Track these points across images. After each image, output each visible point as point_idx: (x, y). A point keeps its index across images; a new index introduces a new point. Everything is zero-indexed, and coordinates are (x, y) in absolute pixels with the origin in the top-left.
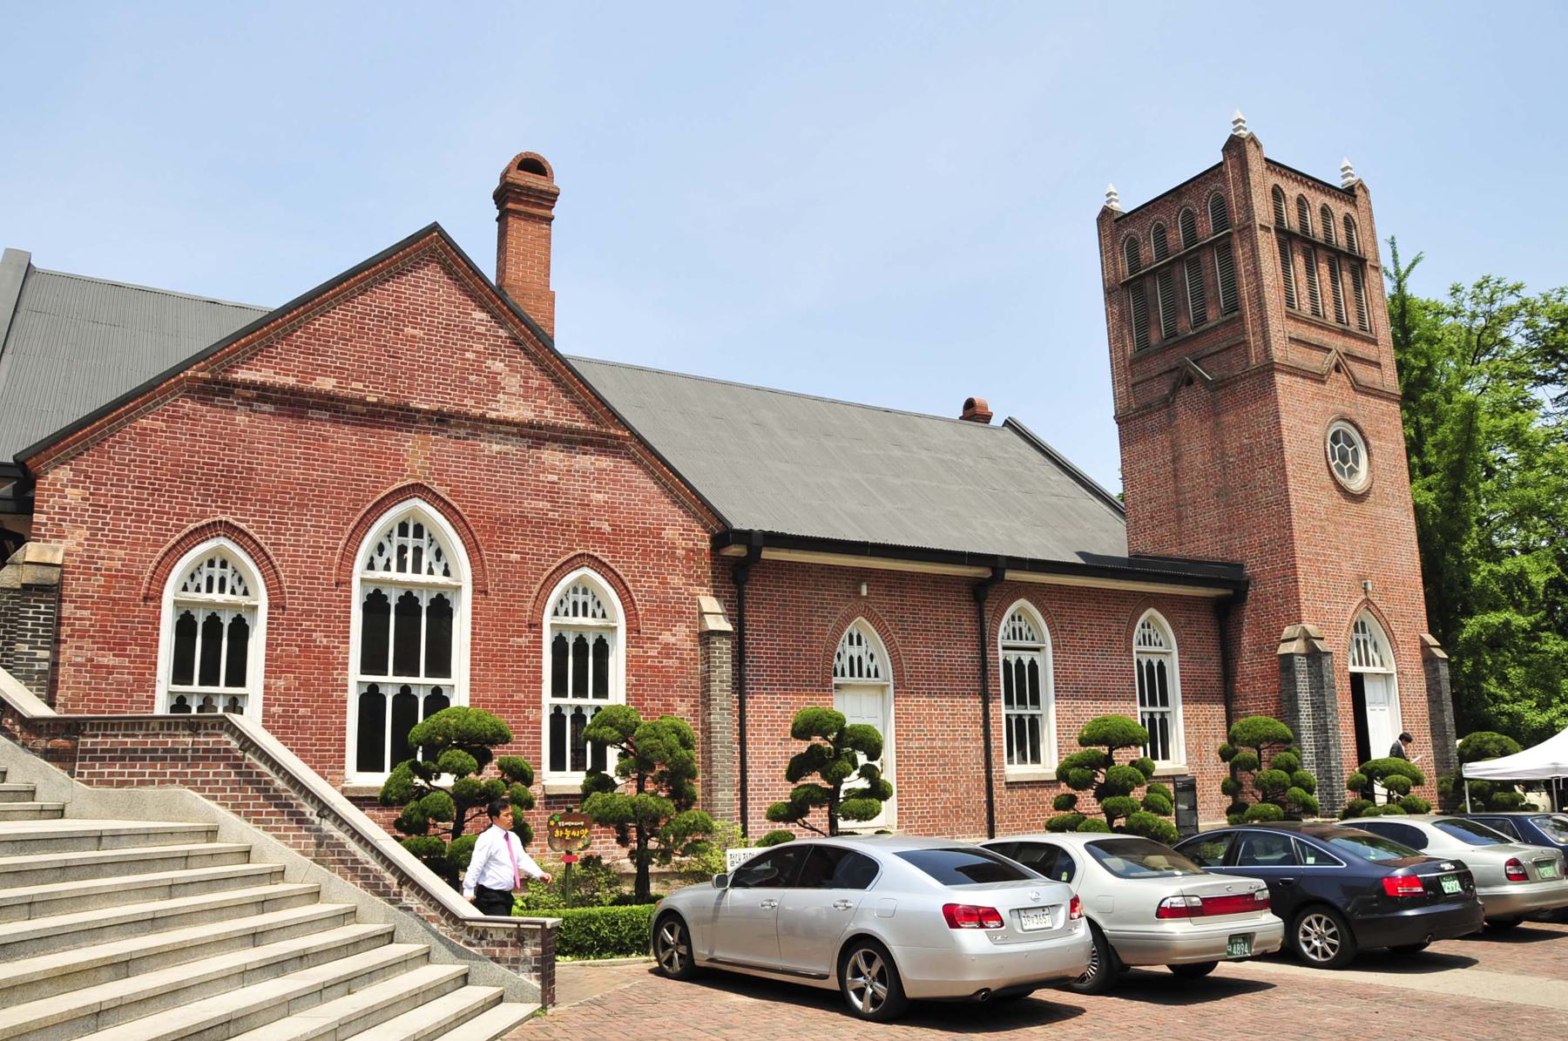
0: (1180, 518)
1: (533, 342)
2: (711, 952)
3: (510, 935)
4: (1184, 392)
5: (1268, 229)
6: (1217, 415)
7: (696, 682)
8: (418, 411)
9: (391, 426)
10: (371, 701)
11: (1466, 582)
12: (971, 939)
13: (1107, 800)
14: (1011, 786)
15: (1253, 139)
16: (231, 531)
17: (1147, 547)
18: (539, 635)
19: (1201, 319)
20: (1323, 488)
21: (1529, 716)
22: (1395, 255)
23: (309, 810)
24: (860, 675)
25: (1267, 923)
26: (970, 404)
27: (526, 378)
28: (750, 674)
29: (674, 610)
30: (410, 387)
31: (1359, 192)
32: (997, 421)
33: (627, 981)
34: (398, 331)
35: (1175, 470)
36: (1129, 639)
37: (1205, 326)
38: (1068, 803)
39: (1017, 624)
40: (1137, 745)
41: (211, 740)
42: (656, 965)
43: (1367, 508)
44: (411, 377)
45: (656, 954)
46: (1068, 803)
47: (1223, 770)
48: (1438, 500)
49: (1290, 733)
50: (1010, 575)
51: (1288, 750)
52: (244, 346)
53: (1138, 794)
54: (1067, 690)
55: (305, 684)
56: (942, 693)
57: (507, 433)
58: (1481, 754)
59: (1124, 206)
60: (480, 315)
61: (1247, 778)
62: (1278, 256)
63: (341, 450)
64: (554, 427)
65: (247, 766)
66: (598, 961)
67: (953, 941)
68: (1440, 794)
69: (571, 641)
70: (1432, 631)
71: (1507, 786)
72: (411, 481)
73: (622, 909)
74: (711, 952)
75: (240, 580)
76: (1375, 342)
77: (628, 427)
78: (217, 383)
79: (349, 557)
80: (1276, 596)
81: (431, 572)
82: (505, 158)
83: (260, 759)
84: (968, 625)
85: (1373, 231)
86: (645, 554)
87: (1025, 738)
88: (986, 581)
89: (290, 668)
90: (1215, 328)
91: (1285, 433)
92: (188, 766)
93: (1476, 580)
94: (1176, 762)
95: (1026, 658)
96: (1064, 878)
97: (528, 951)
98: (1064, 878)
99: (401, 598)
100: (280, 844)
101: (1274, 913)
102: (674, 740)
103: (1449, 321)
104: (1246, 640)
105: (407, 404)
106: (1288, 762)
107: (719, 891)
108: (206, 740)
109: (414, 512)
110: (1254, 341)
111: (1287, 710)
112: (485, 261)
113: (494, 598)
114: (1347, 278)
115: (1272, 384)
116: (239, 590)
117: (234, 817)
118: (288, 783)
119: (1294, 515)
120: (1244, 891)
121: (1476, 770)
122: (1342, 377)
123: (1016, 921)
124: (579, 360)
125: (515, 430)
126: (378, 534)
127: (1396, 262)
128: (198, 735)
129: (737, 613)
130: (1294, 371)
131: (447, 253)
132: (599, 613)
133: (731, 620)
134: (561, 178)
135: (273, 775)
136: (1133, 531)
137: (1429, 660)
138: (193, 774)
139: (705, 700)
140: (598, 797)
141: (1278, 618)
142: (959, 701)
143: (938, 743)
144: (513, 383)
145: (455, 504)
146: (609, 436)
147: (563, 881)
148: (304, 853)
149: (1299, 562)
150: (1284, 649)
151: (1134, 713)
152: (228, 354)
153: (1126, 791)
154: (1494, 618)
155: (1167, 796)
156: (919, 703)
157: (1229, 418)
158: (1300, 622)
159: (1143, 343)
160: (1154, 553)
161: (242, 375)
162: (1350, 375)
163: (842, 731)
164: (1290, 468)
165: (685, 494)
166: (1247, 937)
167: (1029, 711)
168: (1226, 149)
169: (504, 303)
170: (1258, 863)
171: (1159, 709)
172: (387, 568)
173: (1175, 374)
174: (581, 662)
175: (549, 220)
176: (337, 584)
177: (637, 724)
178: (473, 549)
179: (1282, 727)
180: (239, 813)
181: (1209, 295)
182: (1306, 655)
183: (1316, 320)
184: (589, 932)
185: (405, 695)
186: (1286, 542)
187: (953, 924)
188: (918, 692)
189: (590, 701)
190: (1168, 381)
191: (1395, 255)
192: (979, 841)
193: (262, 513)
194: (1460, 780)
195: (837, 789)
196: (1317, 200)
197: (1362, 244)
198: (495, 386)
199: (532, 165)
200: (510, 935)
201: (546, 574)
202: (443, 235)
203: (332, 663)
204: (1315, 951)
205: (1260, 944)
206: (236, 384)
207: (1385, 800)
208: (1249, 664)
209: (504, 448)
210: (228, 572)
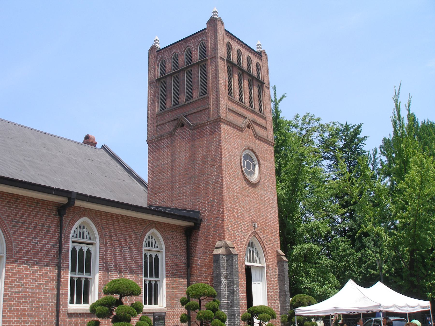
0: (172, 189)
4: (180, 130)
11: (295, 231)
14: (71, 315)
15: (221, 20)
17: (157, 202)
20: (238, 179)
21: (317, 288)
22: (275, 93)
26: (87, 137)
31: (263, 55)
32: (99, 146)
35: (172, 166)
39: (82, 230)
43: (257, 190)
48: (286, 194)
49: (216, 293)
50: (78, 203)
51: (214, 300)
58: (301, 304)
61: (194, 315)
68: (282, 322)
70: (282, 249)
71: (309, 318)
76: (265, 119)
84: (53, 227)
85: (268, 72)
87: (80, 291)
88: (65, 205)
90: (196, 101)
91: (223, 151)
93: (299, 230)
95: (85, 248)
103: (294, 129)
106: (214, 307)
110: (213, 108)
111: (215, 281)
114: (255, 89)
115: (219, 128)
119: (224, 189)
121: (302, 311)
122: (250, 131)
127: (275, 96)
130: (229, 124)
136: (150, 195)
137: (280, 261)
141: (214, 237)
142: (44, 268)
149: (225, 211)
150: (216, 252)
154: (306, 246)
156: (21, 268)
157: (198, 143)
158: (224, 239)
159: (163, 107)
160: (159, 205)
162: (254, 130)
164: (224, 167)
167: (84, 276)
168: (209, 23)
171: (154, 279)
173: (176, 122)
179: (212, 290)
181: (194, 86)
182: (226, 256)
188: (20, 261)
190: (173, 124)
191: (275, 93)
194: (293, 315)
196: (246, 54)
197: (263, 76)
208: (199, 259)
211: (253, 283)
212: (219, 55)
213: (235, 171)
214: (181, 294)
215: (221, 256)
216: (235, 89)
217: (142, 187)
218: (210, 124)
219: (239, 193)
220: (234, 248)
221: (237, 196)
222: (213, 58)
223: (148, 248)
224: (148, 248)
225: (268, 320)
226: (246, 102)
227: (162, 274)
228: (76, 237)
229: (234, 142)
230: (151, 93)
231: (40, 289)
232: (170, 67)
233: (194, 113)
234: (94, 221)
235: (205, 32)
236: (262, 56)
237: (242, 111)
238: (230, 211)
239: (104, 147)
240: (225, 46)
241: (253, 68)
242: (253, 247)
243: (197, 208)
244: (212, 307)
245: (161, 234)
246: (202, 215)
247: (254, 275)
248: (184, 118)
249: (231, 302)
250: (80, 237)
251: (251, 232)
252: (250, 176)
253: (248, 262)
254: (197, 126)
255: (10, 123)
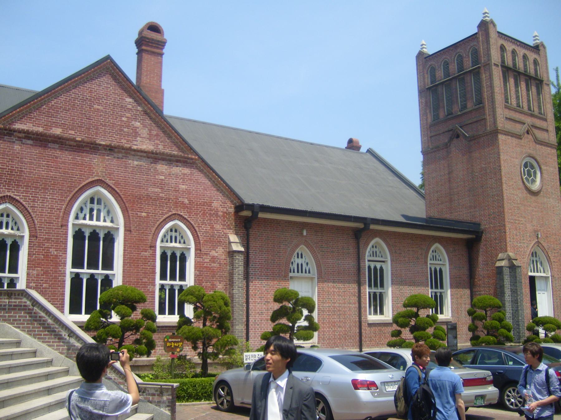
0: (451, 201)
1: (152, 111)
2: (243, 399)
3: (156, 391)
4: (455, 141)
5: (497, 66)
6: (470, 152)
7: (226, 274)
8: (100, 145)
9: (87, 152)
10: (76, 280)
12: (364, 395)
13: (416, 333)
14: (371, 325)
15: (492, 22)
16: (12, 200)
17: (435, 214)
18: (155, 251)
19: (464, 107)
20: (519, 189)
23: (64, 334)
24: (302, 272)
25: (491, 390)
26: (350, 141)
27: (150, 130)
28: (251, 271)
29: (216, 241)
30: (97, 133)
31: (541, 48)
32: (363, 150)
33: (203, 412)
34: (91, 107)
35: (449, 178)
36: (426, 257)
37: (466, 111)
38: (397, 334)
39: (375, 249)
40: (430, 308)
41: (18, 301)
42: (216, 405)
43: (540, 199)
44: (97, 129)
45: (216, 400)
46: (397, 334)
47: (468, 320)
49: (500, 304)
50: (372, 227)
51: (499, 312)
52: (19, 112)
53: (430, 331)
54: (397, 281)
55: (46, 273)
56: (340, 282)
57: (141, 156)
59: (430, 50)
60: (129, 100)
62: (502, 79)
63: (64, 163)
64: (163, 154)
65: (35, 313)
66: (187, 403)
67: (357, 397)
69: (169, 254)
72: (96, 178)
73: (198, 380)
74: (243, 399)
75: (16, 223)
76: (546, 120)
77: (197, 154)
78: (6, 130)
79: (67, 213)
80: (495, 239)
81: (105, 221)
82: (142, 24)
83: (41, 310)
86: (204, 214)
87: (377, 302)
88: (360, 230)
89: (39, 265)
90: (471, 112)
91: (502, 162)
92: (7, 313)
94: (446, 315)
95: (378, 265)
96: (402, 368)
97: (165, 398)
98: (402, 368)
99: (91, 233)
100: (50, 349)
101: (495, 386)
102: (222, 303)
104: (481, 259)
105: (95, 142)
106: (499, 318)
107: (246, 372)
108: (15, 301)
109: (98, 192)
110: (489, 119)
111: (499, 292)
112: (131, 73)
113: (134, 234)
114: (534, 89)
115: (497, 139)
116: (15, 228)
117: (28, 336)
118: (54, 321)
119: (505, 201)
120: (482, 376)
122: (530, 137)
123: (383, 387)
124: (171, 117)
125: (145, 155)
126: (81, 202)
128: (11, 298)
129: (246, 243)
130: (507, 133)
131: (114, 69)
132: (182, 241)
133: (243, 246)
134: (168, 35)
135: (47, 318)
136: (429, 205)
138: (9, 316)
139: (231, 283)
140: (185, 328)
141: (496, 250)
143: (337, 305)
144: (144, 132)
145: (116, 189)
146: (188, 158)
147: (171, 366)
148: (61, 353)
150: (498, 264)
151: (429, 292)
152: (11, 116)
153: (424, 329)
155: (443, 331)
158: (506, 251)
160: (438, 217)
161: (18, 126)
162: (534, 135)
163: (297, 300)
164: (504, 179)
165: (223, 186)
166: (482, 397)
167: (379, 290)
169: (141, 94)
170: (486, 364)
171: (439, 290)
172: (84, 218)
173: (451, 133)
174: (174, 263)
175: (161, 55)
176: (62, 226)
177: (204, 295)
178: (125, 211)
179: (497, 301)
180: (30, 335)
182: (509, 267)
183: (518, 109)
184: (183, 390)
185: (92, 279)
186: (501, 214)
187: (356, 388)
188: (328, 281)
189: (178, 282)
192: (355, 351)
193: (27, 192)
195: (293, 326)
196: (521, 52)
197: (541, 73)
198: (136, 134)
199: (154, 28)
200: (156, 391)
201: (158, 223)
202: (112, 61)
203: (59, 263)
204: (512, 404)
205: (487, 400)
206: (15, 131)
207: (544, 335)
208: (482, 270)
209: (140, 163)
210: (10, 220)
211: (537, 292)
212: (493, 62)
213: (515, 182)
214: (465, 304)
215: (504, 268)
216: (512, 95)
217: (412, 191)
218: (487, 135)
219: (521, 204)
220: (517, 260)
221: (518, 207)
222: (486, 65)
223: (432, 262)
224: (432, 262)
225: (554, 330)
226: (524, 106)
227: (447, 285)
228: (370, 256)
229: (513, 152)
230: (422, 102)
231: (345, 303)
232: (440, 74)
233: (470, 124)
234: (384, 240)
235: (476, 37)
236: (539, 50)
237: (520, 117)
238: (512, 223)
239: (369, 151)
240: (499, 49)
241: (531, 66)
242: (536, 256)
243: (477, 220)
244: (498, 318)
245: (444, 248)
246: (482, 227)
247: (539, 285)
248: (459, 129)
249: (516, 312)
250: (373, 256)
251: (534, 242)
252: (532, 183)
253: (531, 272)
254: (473, 137)
255: (278, 137)
